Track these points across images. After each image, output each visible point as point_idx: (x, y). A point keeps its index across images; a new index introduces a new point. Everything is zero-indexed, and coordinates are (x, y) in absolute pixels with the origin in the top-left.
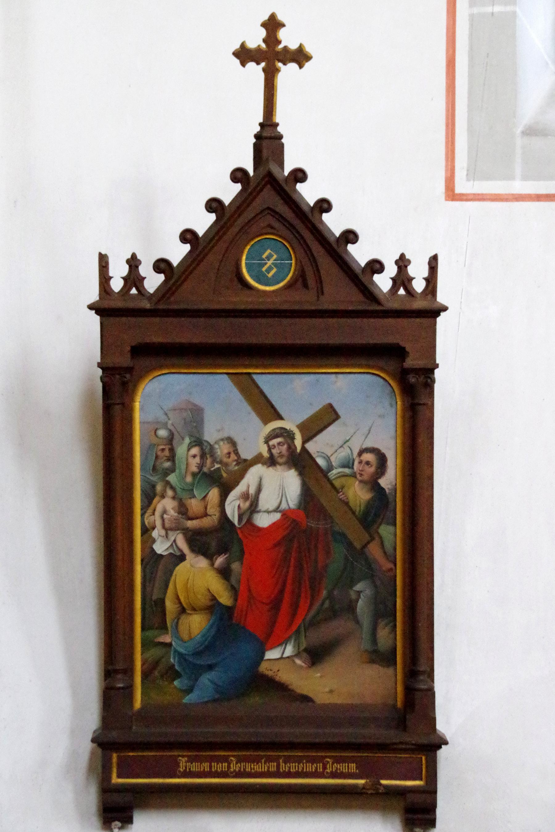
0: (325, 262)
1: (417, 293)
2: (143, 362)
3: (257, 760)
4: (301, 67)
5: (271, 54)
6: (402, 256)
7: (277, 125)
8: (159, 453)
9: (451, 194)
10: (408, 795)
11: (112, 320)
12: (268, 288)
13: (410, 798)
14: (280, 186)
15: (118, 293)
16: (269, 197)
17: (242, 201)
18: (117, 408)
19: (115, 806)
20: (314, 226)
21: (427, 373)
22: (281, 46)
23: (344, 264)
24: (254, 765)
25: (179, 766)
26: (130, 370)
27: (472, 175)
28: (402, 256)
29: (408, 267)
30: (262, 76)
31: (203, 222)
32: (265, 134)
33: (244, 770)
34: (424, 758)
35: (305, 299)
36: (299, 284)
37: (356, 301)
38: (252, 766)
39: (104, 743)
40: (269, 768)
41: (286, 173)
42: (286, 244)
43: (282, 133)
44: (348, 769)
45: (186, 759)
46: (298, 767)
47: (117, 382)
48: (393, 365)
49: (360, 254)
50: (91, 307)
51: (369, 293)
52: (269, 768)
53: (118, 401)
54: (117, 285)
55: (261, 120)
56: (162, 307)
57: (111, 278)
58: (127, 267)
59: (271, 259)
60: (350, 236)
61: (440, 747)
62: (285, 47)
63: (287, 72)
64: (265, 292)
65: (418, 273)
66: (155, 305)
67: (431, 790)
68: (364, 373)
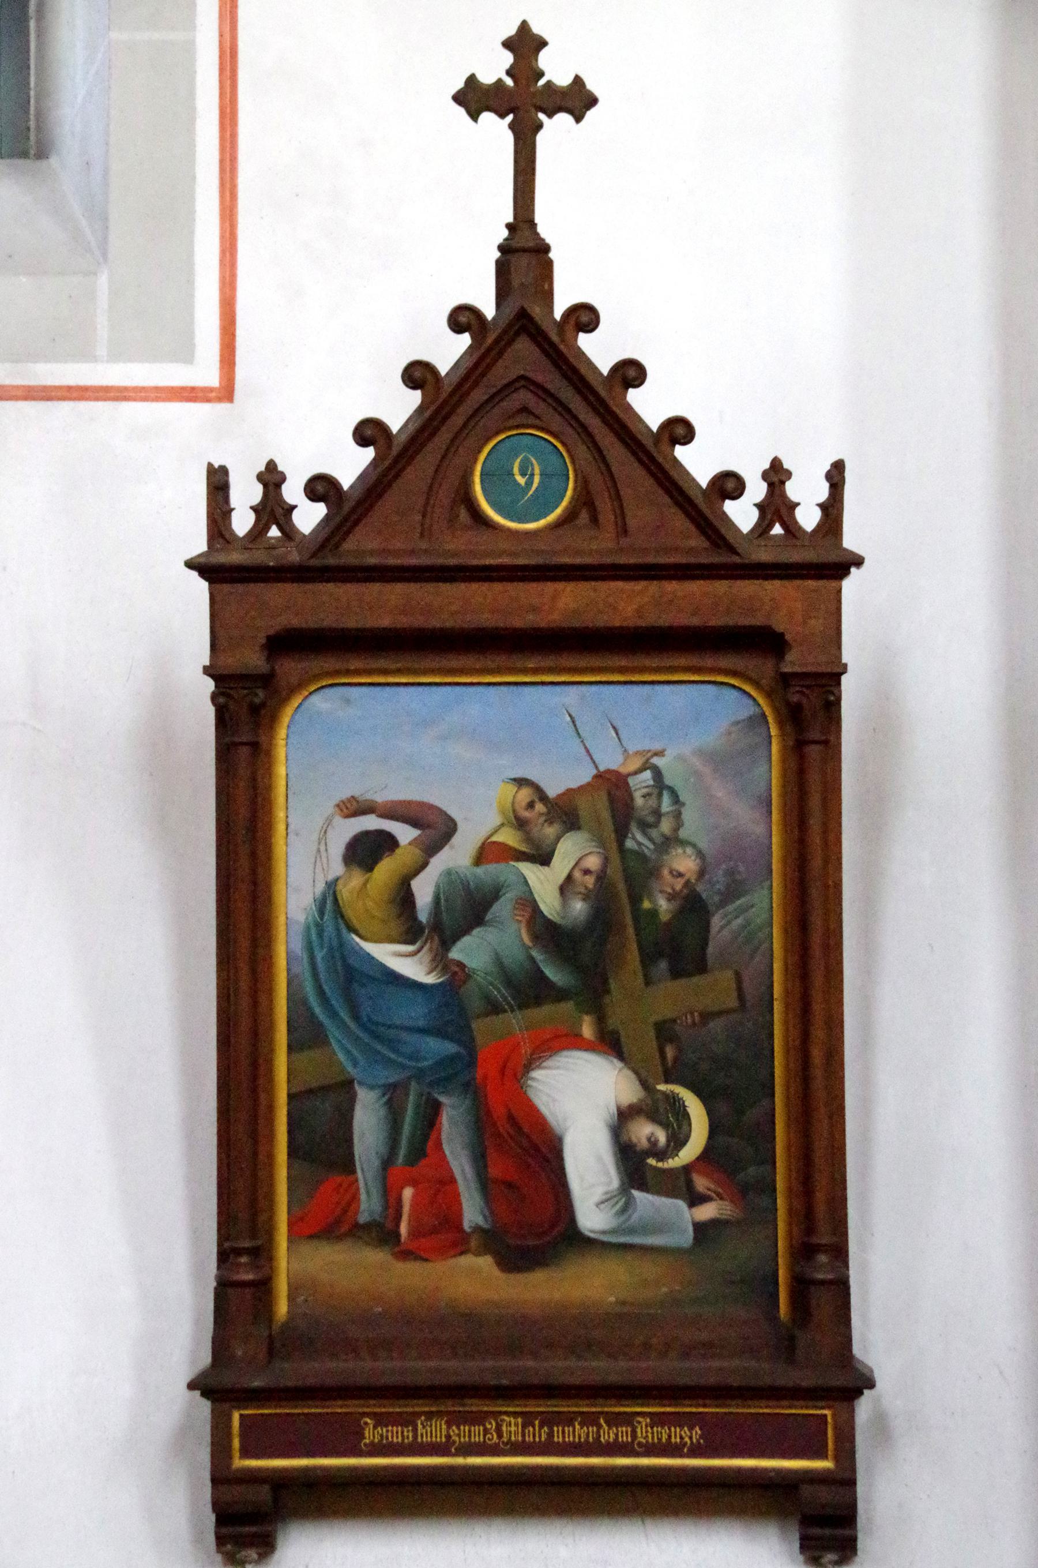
1: (804, 531)
2: (289, 668)
3: (408, 1421)
4: (578, 119)
9: (226, 392)
11: (226, 588)
15: (244, 537)
16: (526, 358)
17: (474, 368)
19: (245, 1515)
21: (829, 679)
22: (541, 82)
23: (672, 482)
26: (266, 680)
27: (186, 354)
29: (788, 484)
30: (509, 138)
31: (399, 408)
32: (515, 244)
35: (595, 545)
36: (584, 516)
37: (692, 545)
38: (405, 1434)
40: (617, 1435)
41: (558, 315)
43: (548, 241)
44: (564, 1437)
45: (648, 1420)
47: (246, 706)
48: (764, 667)
50: (190, 565)
51: (714, 530)
52: (617, 1435)
54: (242, 522)
55: (510, 219)
56: (319, 564)
57: (233, 509)
59: (528, 473)
60: (680, 430)
61: (859, 1393)
63: (555, 131)
64: (527, 534)
67: (844, 1481)
68: (625, 683)
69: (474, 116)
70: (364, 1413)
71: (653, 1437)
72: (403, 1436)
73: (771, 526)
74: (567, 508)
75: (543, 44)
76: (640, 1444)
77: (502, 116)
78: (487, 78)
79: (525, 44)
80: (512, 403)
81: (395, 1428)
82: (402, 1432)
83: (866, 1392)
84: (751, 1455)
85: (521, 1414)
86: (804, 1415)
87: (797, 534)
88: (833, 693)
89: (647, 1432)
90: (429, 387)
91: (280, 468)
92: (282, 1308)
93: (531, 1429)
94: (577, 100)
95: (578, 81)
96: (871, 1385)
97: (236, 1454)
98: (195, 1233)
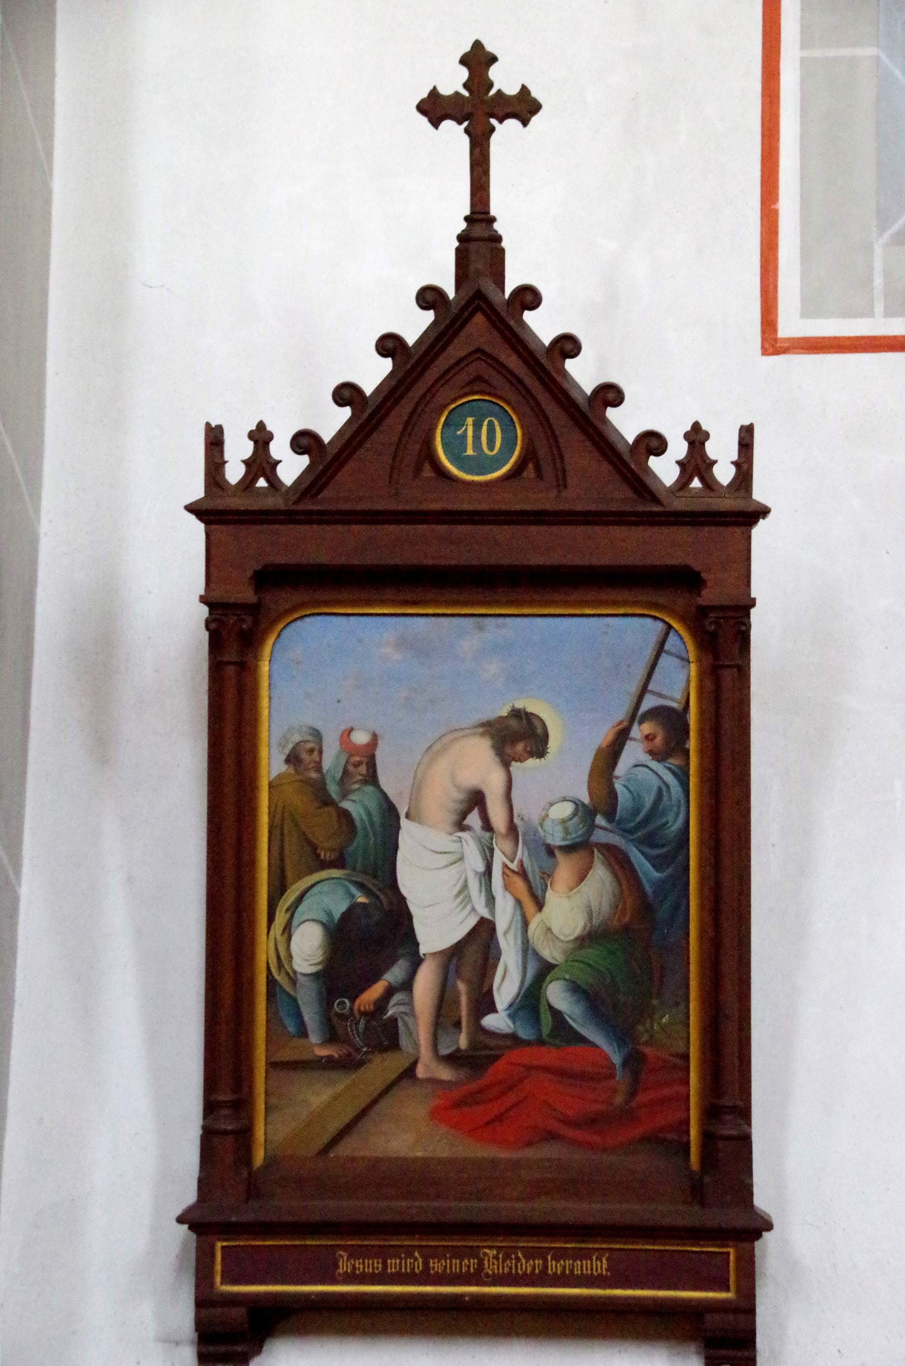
0: (572, 439)
4: (525, 123)
5: (478, 105)
6: (696, 427)
7: (494, 220)
8: (351, 768)
10: (708, 1317)
12: (476, 478)
13: (712, 1321)
14: (498, 314)
16: (477, 332)
17: (436, 340)
18: (231, 670)
20: (596, 429)
22: (493, 92)
23: (602, 440)
24: (434, 1263)
25: (337, 1267)
26: (254, 609)
28: (696, 427)
30: (466, 140)
33: (572, 1271)
35: (543, 499)
37: (619, 497)
39: (200, 1222)
41: (507, 295)
42: (507, 408)
43: (500, 232)
46: (556, 1267)
47: (235, 633)
48: (681, 601)
49: (626, 422)
50: (190, 508)
51: (641, 484)
53: (234, 658)
54: (234, 473)
55: (467, 212)
56: (306, 505)
58: (251, 444)
61: (758, 1235)
62: (499, 92)
63: (506, 134)
64: (487, 484)
65: (722, 452)
66: (293, 504)
68: (453, 615)
69: (436, 123)
70: (338, 1246)
72: (373, 1267)
73: (690, 480)
74: (516, 463)
75: (493, 59)
77: (460, 123)
78: (446, 90)
79: (478, 60)
80: (474, 369)
82: (373, 1264)
83: (765, 1234)
84: (669, 1288)
85: (499, 1248)
86: (678, 1251)
87: (715, 487)
88: (744, 624)
89: (493, 1264)
90: (398, 357)
92: (259, 1157)
94: (524, 107)
95: (524, 90)
96: (769, 1227)
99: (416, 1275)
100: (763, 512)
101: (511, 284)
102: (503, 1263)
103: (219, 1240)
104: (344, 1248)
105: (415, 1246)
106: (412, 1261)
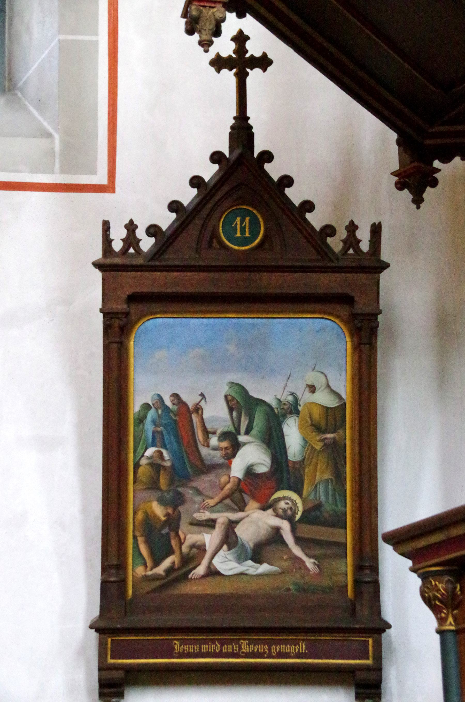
2: (135, 309)
7: (249, 118)
9: (109, 188)
10: (357, 673)
13: (360, 675)
17: (221, 180)
19: (111, 684)
22: (234, 56)
25: (175, 650)
26: (127, 314)
33: (215, 650)
34: (370, 640)
37: (308, 256)
41: (255, 155)
43: (251, 125)
48: (344, 311)
51: (324, 251)
52: (280, 649)
54: (117, 246)
56: (155, 262)
58: (126, 231)
61: (384, 631)
63: (254, 76)
65: (364, 235)
67: (377, 669)
69: (218, 71)
71: (249, 649)
73: (348, 249)
76: (243, 652)
81: (205, 646)
83: (387, 630)
89: (247, 647)
91: (135, 223)
93: (298, 646)
97: (109, 657)
98: (88, 560)
99: (217, 653)
100: (386, 266)
101: (257, 151)
102: (180, 646)
103: (109, 637)
104: (177, 640)
105: (216, 639)
106: (214, 646)
